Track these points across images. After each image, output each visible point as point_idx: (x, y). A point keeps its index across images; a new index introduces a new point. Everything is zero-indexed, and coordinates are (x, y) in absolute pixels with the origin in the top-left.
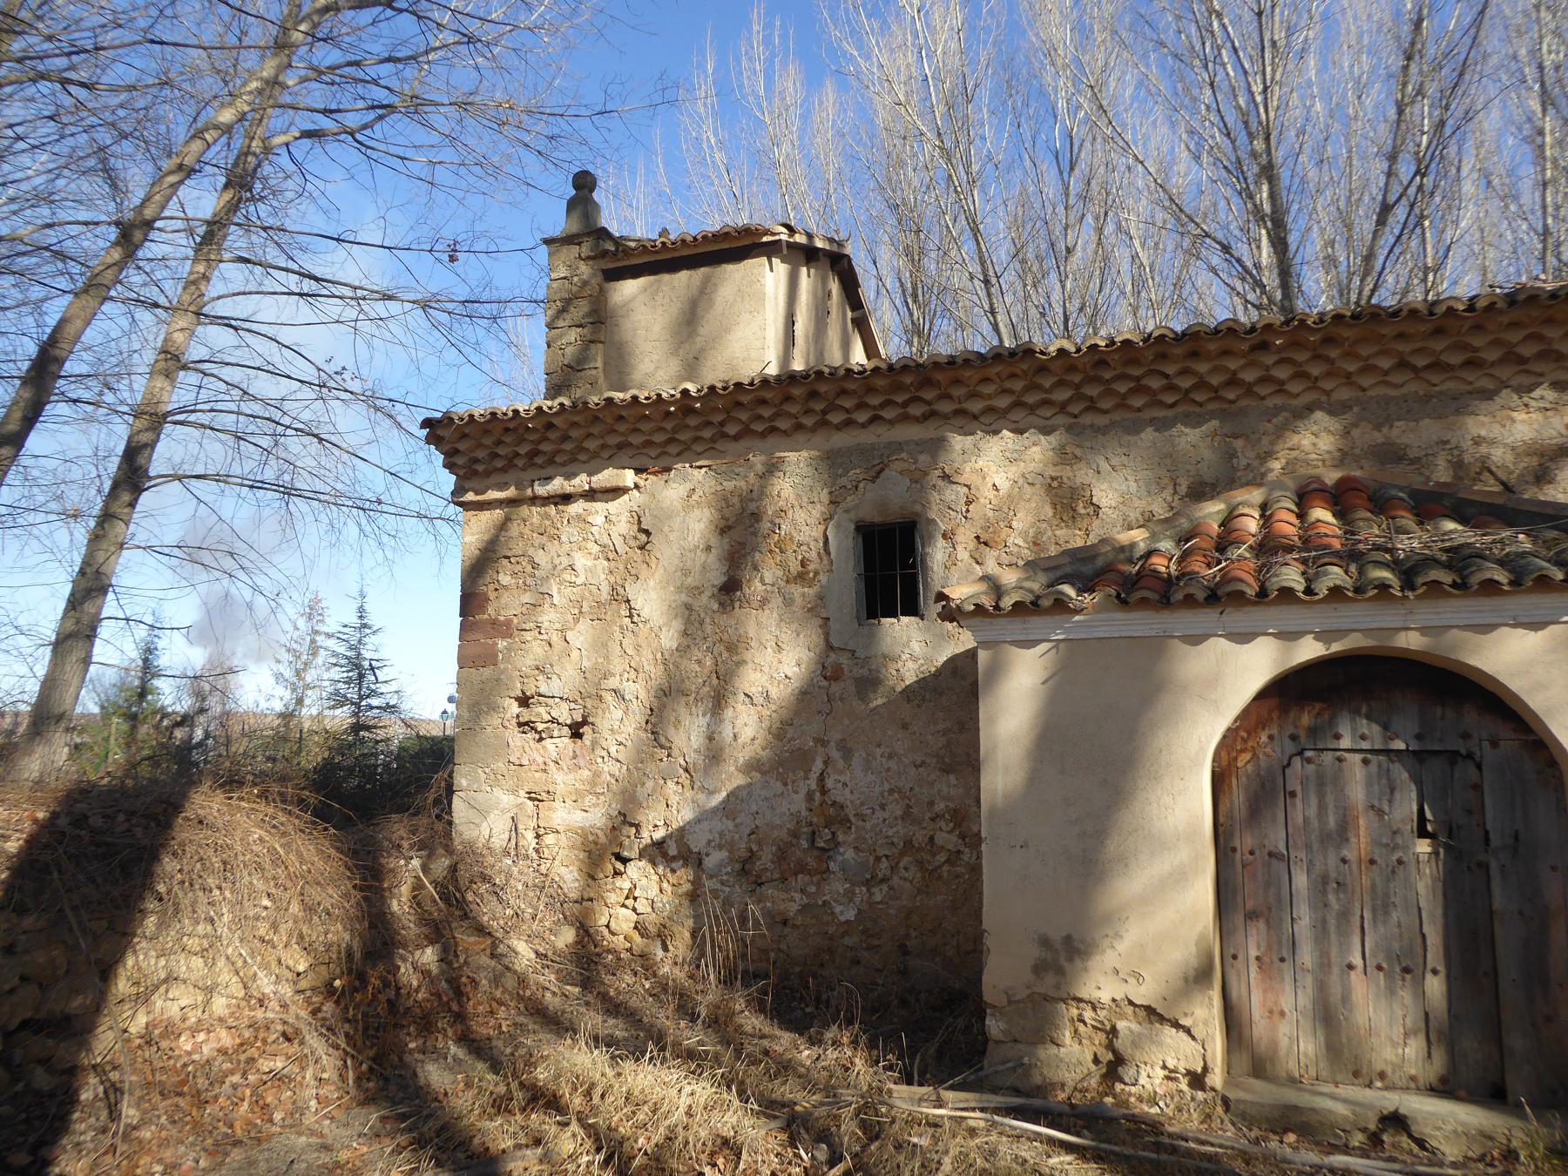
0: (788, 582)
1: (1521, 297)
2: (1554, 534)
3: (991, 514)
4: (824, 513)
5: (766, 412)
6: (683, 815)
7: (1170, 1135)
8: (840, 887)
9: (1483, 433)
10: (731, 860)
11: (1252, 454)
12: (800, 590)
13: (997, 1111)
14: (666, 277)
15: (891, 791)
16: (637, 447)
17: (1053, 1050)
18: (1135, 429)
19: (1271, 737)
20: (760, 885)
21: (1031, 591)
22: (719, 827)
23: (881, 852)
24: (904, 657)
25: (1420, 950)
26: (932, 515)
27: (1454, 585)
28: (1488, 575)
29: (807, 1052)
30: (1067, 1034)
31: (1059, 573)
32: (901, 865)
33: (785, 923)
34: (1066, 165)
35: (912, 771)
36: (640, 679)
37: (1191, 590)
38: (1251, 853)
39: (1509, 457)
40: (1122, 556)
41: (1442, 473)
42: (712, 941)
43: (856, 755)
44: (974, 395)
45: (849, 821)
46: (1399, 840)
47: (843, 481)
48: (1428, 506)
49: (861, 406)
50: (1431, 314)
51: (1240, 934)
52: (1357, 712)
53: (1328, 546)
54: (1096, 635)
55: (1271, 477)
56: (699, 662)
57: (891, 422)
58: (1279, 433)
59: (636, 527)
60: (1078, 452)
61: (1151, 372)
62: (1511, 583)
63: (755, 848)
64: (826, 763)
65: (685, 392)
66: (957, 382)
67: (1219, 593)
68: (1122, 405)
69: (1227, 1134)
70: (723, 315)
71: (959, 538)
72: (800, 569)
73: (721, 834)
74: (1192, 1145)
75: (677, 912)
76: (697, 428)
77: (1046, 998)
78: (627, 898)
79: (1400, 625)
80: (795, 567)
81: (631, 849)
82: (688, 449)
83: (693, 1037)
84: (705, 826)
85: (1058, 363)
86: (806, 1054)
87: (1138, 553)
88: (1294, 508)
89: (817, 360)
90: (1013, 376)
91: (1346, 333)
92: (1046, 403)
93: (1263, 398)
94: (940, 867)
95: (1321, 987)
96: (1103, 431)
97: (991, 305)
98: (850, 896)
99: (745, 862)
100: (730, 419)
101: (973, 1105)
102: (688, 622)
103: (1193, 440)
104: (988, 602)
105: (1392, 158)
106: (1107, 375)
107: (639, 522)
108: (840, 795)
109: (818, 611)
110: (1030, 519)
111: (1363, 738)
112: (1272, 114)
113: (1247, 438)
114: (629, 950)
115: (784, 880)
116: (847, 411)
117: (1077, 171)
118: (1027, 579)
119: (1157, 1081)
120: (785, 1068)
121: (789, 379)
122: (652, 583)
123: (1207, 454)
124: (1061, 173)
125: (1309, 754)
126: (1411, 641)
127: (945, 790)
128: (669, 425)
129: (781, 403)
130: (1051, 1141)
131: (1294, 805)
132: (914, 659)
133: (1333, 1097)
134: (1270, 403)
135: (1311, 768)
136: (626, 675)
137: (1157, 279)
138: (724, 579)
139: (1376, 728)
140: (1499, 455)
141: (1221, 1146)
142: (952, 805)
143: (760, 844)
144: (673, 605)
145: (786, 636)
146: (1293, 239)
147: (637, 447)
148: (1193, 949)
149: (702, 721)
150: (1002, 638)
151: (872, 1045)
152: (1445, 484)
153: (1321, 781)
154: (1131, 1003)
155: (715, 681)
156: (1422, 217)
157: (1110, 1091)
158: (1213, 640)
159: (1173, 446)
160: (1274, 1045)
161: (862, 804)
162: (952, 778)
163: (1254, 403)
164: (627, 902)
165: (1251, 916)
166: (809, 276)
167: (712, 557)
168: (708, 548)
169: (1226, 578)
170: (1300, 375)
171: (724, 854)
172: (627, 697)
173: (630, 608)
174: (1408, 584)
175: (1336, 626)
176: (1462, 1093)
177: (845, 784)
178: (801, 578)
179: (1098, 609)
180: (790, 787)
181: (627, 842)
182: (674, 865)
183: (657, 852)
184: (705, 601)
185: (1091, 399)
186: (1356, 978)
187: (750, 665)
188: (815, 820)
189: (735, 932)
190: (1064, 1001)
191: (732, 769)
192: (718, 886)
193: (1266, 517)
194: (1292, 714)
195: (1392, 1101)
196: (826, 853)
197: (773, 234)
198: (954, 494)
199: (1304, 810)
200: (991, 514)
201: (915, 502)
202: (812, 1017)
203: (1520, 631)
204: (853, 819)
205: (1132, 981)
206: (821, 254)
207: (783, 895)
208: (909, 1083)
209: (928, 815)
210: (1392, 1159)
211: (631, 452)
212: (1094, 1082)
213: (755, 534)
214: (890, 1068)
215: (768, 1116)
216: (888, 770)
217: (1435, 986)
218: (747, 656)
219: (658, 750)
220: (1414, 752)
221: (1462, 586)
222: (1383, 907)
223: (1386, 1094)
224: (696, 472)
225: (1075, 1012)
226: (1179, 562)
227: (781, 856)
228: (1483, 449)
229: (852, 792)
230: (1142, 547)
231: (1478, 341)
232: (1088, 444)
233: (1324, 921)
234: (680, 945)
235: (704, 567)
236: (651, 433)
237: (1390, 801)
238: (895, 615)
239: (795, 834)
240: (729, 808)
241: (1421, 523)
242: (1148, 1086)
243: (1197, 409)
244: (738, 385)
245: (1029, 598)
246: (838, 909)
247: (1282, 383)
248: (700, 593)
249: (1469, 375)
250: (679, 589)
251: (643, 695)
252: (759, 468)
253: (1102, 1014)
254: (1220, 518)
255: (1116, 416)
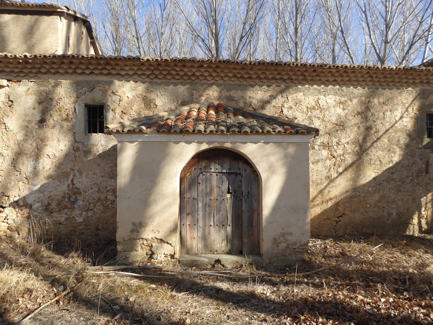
0: (62, 121)
1: (261, 63)
2: (262, 121)
3: (126, 105)
4: (74, 100)
5: (55, 66)
6: (24, 192)
7: (164, 271)
8: (78, 212)
9: (251, 96)
10: (42, 206)
11: (197, 95)
12: (66, 123)
13: (119, 270)
14: (21, 16)
15: (94, 184)
16: (7, 72)
17: (135, 252)
18: (168, 85)
19: (195, 169)
20: (52, 213)
21: (133, 127)
22: (38, 196)
23: (91, 202)
24: (99, 145)
25: (226, 221)
26: (109, 104)
27: (238, 132)
28: (245, 130)
29: (63, 261)
30: (139, 248)
31: (142, 123)
32: (97, 205)
33: (60, 224)
34: (163, 8)
35: (101, 178)
36: (9, 150)
37: (176, 129)
38: (189, 198)
39: (256, 102)
40: (160, 119)
41: (241, 105)
42: (33, 230)
43: (84, 173)
44: (122, 69)
45: (81, 193)
46: (223, 194)
47: (81, 91)
48: (237, 112)
49: (87, 68)
50: (241, 64)
51: (185, 220)
52: (215, 163)
53: (211, 120)
54: (151, 140)
55: (202, 101)
56: (31, 144)
57: (97, 74)
58: (204, 90)
59: (8, 99)
60: (152, 89)
61: (173, 69)
62: (250, 132)
63: (50, 202)
64: (74, 176)
65: (25, 56)
66: (117, 65)
67: (183, 130)
68: (165, 78)
69: (179, 269)
70: (43, 33)
71: (117, 111)
72: (66, 117)
73: (39, 198)
74: (169, 273)
75: (23, 223)
76: (30, 69)
77: (134, 239)
78: (5, 219)
79: (226, 141)
80: (64, 116)
81: (6, 204)
82: (27, 75)
83: (22, 260)
84: (33, 196)
85: (147, 63)
86: (63, 261)
87: (165, 119)
88: (206, 110)
89: (77, 52)
90: (134, 65)
91: (222, 66)
92: (144, 74)
93: (201, 80)
94: (108, 205)
95: (204, 231)
96: (160, 84)
97: (139, 46)
98: (81, 215)
99: (47, 206)
100: (42, 67)
101: (112, 269)
102: (27, 131)
103: (182, 89)
104: (120, 129)
105: (244, 24)
106: (161, 69)
107: (9, 98)
108: (78, 185)
109: (72, 131)
110: (138, 107)
111: (217, 169)
112: (217, 6)
113: (197, 90)
114: (6, 236)
115: (60, 211)
116: (83, 69)
117: (166, 11)
118: (133, 124)
119: (162, 258)
120: (55, 266)
121: (64, 56)
122: (14, 118)
123: (186, 94)
124: (161, 10)
125: (204, 173)
126: (228, 145)
127: (110, 183)
128: (20, 66)
129: (60, 64)
130: (132, 276)
131: (200, 186)
132: (102, 146)
133: (205, 257)
134: (203, 82)
135: (204, 176)
136: (4, 148)
137: (186, 46)
138: (40, 118)
139: (220, 167)
140: (254, 101)
141: (176, 272)
142: (112, 188)
143: (52, 200)
144: (22, 126)
145: (61, 137)
146: (220, 41)
147: (7, 72)
148: (173, 223)
149: (32, 163)
150: (125, 140)
151: (84, 256)
152: (242, 107)
153: (206, 181)
154: (156, 238)
155: (37, 151)
156: (250, 41)
157: (150, 262)
158: (181, 143)
159: (178, 91)
160: (192, 246)
161: (85, 188)
162: (113, 180)
163: (199, 81)
164: (4, 221)
165: (188, 214)
166: (75, 25)
167: (35, 111)
168: (34, 108)
169: (185, 127)
170: (210, 75)
171: (40, 204)
172: (4, 155)
173: (6, 126)
174: (228, 131)
175: (211, 141)
176: (233, 253)
177: (80, 182)
178: (67, 120)
179: (151, 133)
180: (62, 183)
181: (4, 202)
182: (22, 208)
183: (16, 205)
184: (33, 125)
185: (156, 75)
186: (212, 228)
187: (49, 146)
188: (70, 193)
189: (41, 227)
190: (139, 239)
191: (43, 178)
192: (38, 214)
193: (199, 112)
194: (200, 163)
195: (217, 257)
196: (74, 203)
197: (61, 9)
198: (116, 98)
199: (201, 187)
200: (126, 105)
201: (103, 99)
202: (67, 250)
203: (252, 144)
204: (82, 192)
205: (157, 233)
206: (79, 19)
207: (59, 216)
208: (94, 265)
209: (105, 191)
210: (217, 270)
211: (6, 74)
212: (146, 260)
213: (51, 105)
214: (89, 262)
215: (45, 280)
216: (93, 178)
217: (229, 229)
218: (48, 143)
219: (16, 172)
220: (228, 173)
221: (240, 132)
222: (219, 210)
223: (217, 255)
224: (30, 83)
225: (142, 242)
226: (175, 122)
227: (59, 204)
228: (251, 100)
229: (82, 185)
230: (166, 117)
231: (251, 72)
232: (155, 87)
233: (205, 215)
234: (24, 233)
235: (33, 114)
236: (13, 68)
237: (222, 185)
238: (97, 133)
239: (64, 197)
240: (42, 190)
241: (234, 116)
242: (160, 259)
243: (185, 81)
244: (45, 56)
245: (132, 129)
246: (77, 219)
247: (206, 77)
248: (31, 123)
249: (249, 81)
250: (24, 121)
251: (10, 154)
252: (53, 84)
253: (149, 242)
254: (188, 111)
255: (163, 81)
